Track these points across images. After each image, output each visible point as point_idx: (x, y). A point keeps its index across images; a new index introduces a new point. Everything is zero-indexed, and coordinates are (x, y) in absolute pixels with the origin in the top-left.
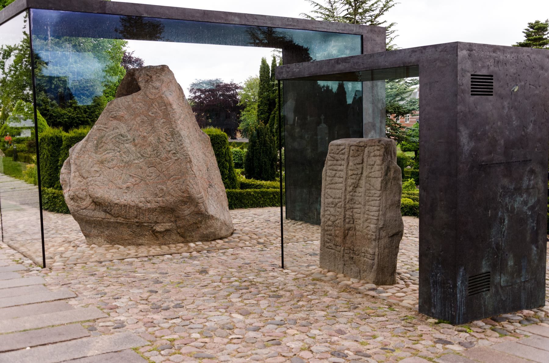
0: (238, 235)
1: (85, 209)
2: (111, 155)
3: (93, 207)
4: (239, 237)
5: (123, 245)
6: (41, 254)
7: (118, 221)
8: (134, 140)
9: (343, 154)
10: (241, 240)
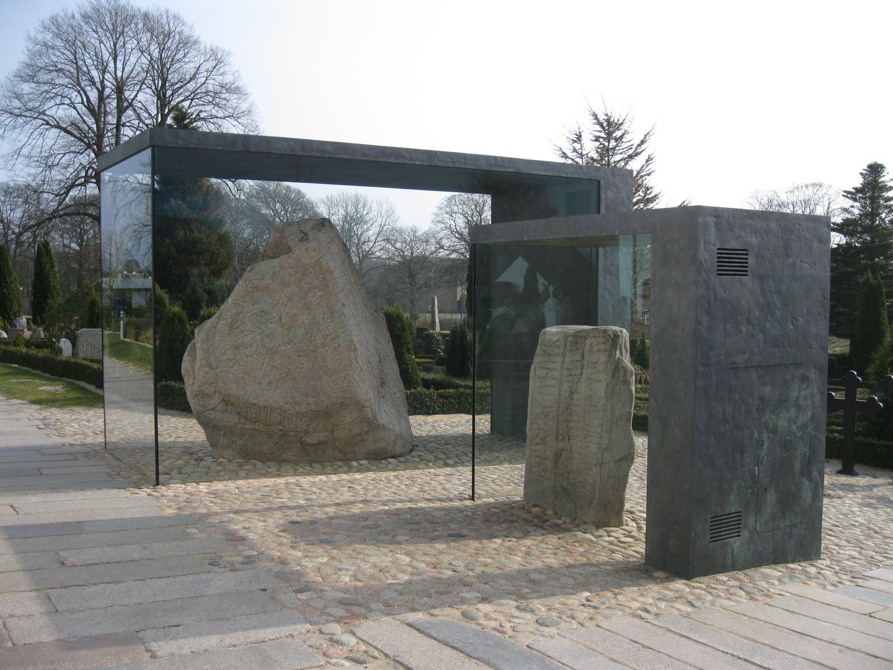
0: (419, 453)
1: (213, 409)
2: (249, 338)
3: (224, 408)
4: (420, 456)
5: (261, 460)
6: (154, 468)
7: (256, 427)
8: (280, 318)
9: (557, 347)
10: (422, 460)
